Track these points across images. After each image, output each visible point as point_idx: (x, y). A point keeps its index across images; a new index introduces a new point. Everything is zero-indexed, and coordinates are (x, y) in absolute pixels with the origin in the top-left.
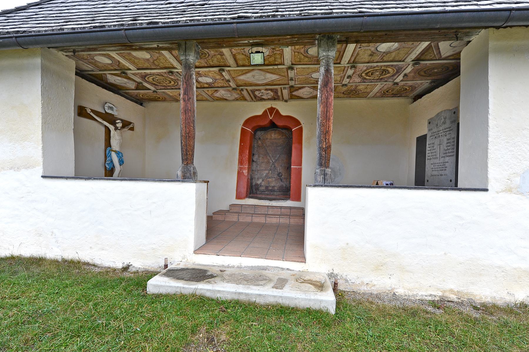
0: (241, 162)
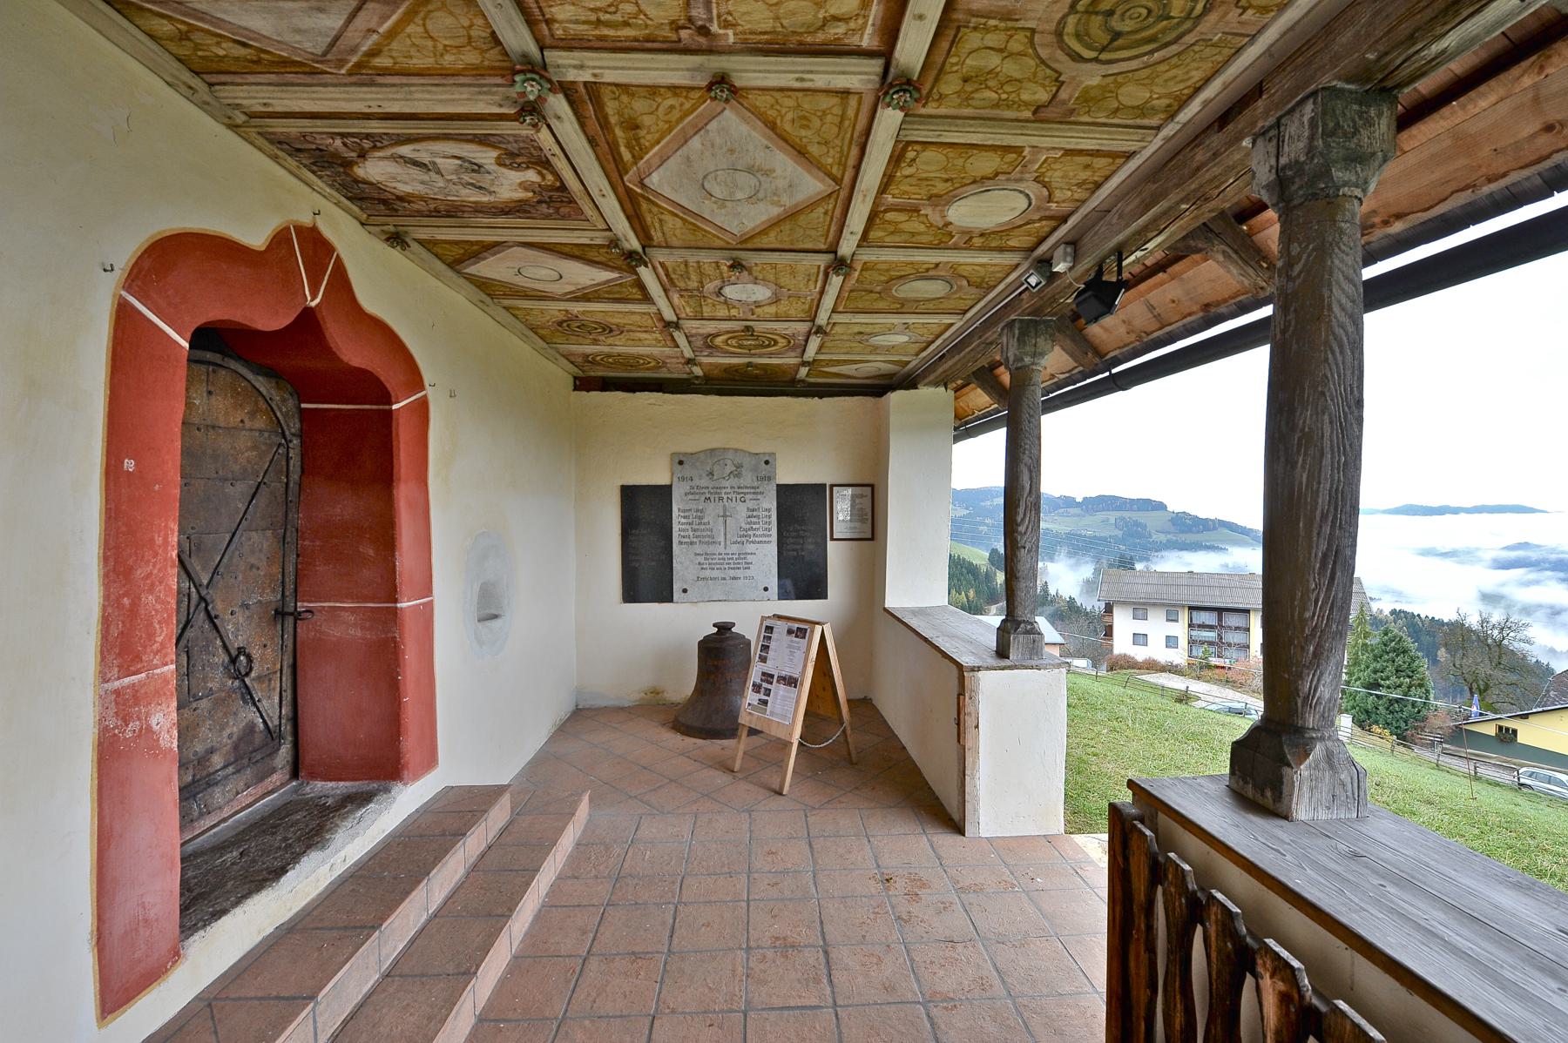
0: (120, 646)
